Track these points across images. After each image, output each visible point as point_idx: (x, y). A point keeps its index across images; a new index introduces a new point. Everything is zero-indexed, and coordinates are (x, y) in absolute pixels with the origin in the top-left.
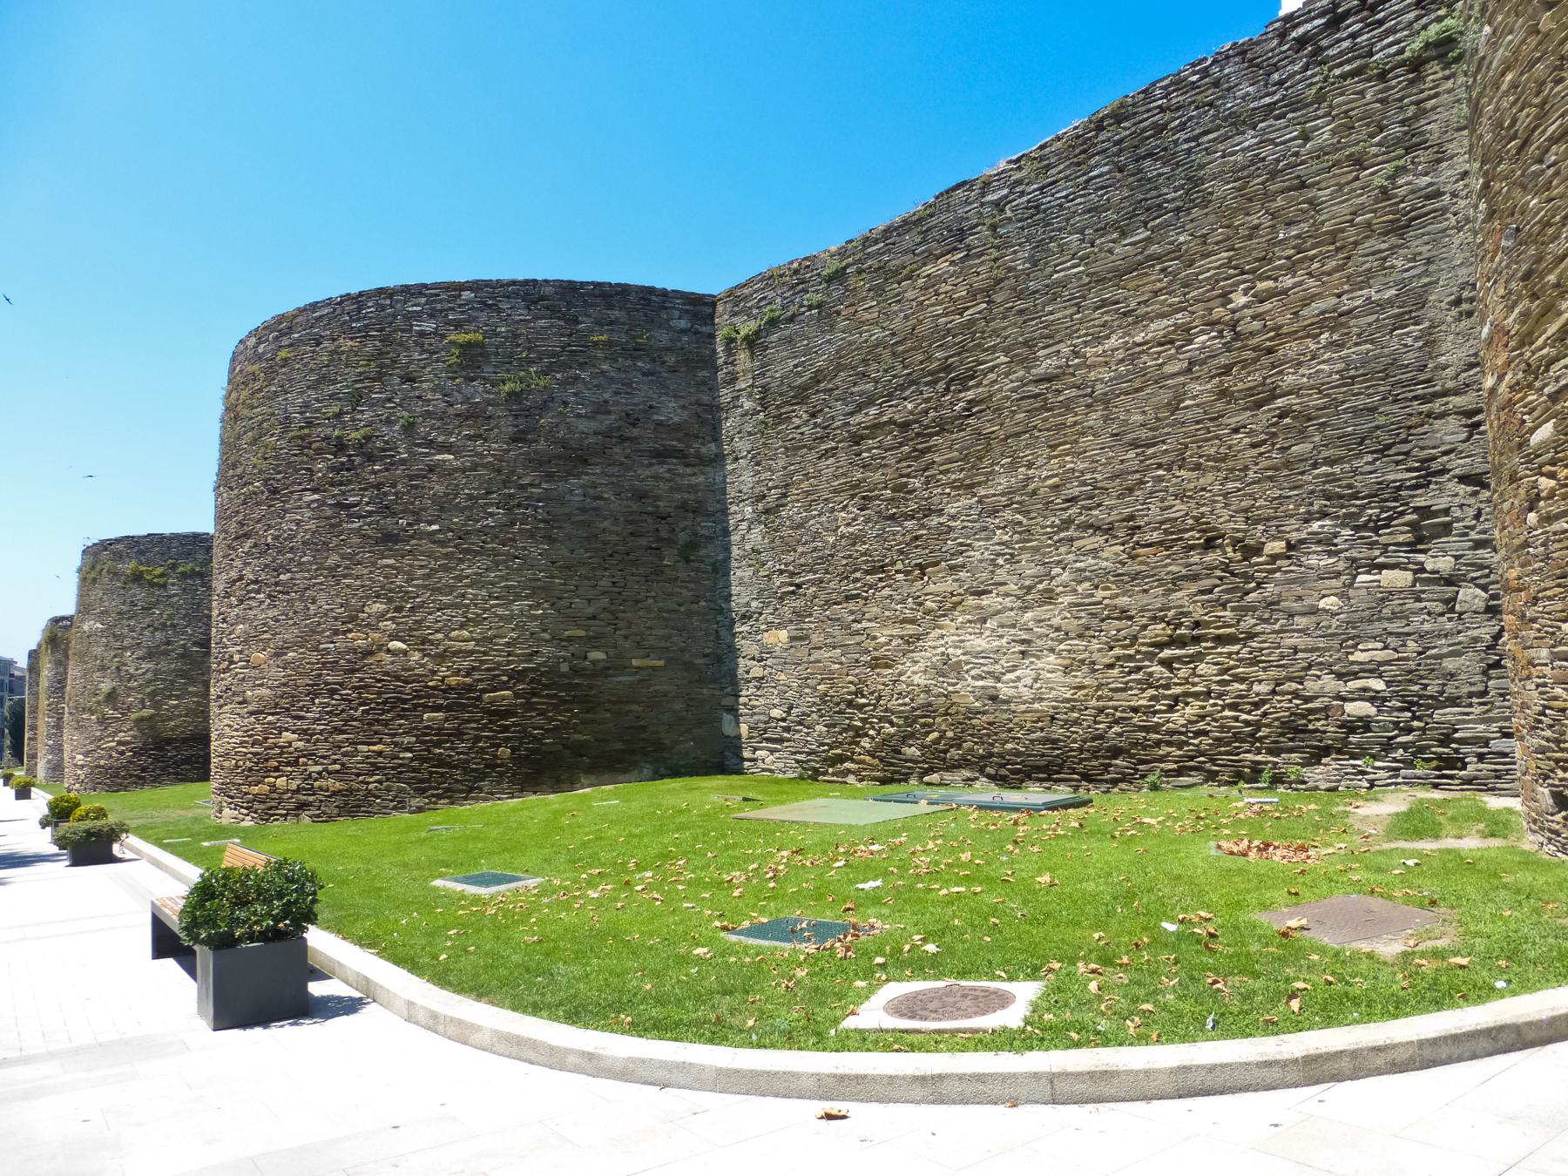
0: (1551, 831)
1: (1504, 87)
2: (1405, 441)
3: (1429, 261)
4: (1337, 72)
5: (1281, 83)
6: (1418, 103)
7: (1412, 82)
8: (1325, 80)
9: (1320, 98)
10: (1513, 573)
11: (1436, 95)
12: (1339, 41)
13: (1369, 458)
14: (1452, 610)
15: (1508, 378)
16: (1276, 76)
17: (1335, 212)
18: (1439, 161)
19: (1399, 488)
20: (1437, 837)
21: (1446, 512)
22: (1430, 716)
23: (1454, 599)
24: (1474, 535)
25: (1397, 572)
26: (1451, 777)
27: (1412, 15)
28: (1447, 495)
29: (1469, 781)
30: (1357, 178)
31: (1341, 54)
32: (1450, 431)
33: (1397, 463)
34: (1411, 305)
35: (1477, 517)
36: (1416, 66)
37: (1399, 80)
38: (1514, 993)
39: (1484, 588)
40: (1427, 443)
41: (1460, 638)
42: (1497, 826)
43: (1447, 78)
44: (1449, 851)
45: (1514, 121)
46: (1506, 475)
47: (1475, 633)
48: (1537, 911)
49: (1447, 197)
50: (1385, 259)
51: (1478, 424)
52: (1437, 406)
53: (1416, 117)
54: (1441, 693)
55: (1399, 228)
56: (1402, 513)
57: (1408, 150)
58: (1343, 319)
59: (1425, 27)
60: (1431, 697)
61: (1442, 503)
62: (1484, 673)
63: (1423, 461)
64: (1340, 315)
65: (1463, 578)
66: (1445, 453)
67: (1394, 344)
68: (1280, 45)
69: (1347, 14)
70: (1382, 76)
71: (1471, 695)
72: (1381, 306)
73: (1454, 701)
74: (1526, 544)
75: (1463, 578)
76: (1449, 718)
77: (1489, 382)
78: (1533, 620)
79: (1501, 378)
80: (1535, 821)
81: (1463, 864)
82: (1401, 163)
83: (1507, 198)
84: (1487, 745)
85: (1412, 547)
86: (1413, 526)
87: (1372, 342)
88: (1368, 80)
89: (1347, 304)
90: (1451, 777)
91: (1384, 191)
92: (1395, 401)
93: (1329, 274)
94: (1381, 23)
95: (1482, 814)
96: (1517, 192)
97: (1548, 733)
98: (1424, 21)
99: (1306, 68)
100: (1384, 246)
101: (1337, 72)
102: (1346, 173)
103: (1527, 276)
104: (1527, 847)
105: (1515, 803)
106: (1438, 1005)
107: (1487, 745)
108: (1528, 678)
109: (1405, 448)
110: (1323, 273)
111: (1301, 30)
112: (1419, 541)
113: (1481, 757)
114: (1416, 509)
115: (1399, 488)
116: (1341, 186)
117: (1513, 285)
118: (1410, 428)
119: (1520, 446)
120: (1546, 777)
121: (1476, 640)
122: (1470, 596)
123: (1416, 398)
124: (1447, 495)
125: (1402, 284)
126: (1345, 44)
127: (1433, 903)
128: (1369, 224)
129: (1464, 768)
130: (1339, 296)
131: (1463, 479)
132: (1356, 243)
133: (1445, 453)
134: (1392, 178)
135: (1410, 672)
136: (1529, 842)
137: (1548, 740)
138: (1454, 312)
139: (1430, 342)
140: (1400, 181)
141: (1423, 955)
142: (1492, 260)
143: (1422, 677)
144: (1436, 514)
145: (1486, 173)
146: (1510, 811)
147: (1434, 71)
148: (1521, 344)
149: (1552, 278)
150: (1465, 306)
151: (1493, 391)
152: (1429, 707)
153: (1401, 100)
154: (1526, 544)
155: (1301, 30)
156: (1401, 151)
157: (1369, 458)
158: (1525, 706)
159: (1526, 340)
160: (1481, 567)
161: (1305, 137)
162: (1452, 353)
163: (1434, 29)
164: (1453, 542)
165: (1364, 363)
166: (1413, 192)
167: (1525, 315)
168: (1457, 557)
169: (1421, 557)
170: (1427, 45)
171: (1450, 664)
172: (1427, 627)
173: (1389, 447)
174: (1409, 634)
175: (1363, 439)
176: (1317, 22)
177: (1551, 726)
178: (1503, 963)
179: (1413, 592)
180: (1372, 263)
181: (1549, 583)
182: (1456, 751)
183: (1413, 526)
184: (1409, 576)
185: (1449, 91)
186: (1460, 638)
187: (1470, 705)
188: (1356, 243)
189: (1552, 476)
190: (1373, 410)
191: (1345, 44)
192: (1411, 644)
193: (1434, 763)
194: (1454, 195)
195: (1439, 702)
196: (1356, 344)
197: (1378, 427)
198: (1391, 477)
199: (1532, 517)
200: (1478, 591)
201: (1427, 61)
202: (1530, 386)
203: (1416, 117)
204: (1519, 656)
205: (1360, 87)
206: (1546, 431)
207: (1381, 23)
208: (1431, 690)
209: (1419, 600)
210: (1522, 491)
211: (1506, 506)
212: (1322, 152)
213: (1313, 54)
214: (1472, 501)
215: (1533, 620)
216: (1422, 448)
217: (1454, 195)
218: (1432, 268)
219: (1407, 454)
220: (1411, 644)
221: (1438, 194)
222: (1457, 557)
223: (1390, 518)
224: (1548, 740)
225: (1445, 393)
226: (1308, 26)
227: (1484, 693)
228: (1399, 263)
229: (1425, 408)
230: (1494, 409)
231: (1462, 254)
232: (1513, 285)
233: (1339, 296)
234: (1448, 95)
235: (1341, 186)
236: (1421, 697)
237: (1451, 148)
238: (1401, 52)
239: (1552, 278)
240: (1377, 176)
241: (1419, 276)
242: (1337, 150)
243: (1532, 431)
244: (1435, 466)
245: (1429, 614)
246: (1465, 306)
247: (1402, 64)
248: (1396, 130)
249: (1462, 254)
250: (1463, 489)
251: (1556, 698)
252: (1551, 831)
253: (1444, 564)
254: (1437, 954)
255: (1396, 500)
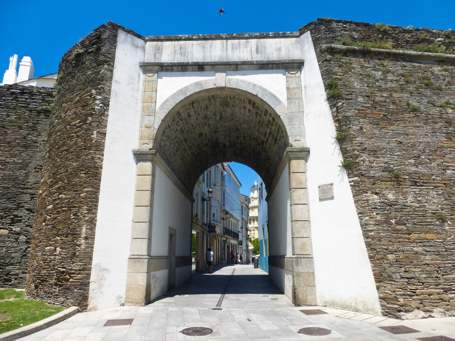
0: (33, 294)
1: (58, 134)
2: (15, 198)
3: (31, 157)
4: (20, 105)
5: (5, 100)
6: (37, 121)
7: (37, 116)
8: (17, 105)
9: (14, 108)
10: (37, 235)
11: (42, 121)
12: (22, 98)
13: (4, 200)
14: (17, 241)
15: (45, 193)
16: (4, 98)
17: (11, 137)
18: (39, 135)
19: (11, 209)
20: (3, 299)
21: (21, 217)
22: (5, 268)
23: (18, 239)
24: (27, 223)
25: (5, 230)
26: (7, 284)
27: (41, 101)
28: (22, 213)
29: (11, 285)
30: (19, 131)
31: (22, 101)
32: (27, 198)
33: (12, 203)
34: (24, 166)
35: (28, 219)
36: (39, 112)
37: (34, 113)
38: (24, 326)
39: (26, 236)
40: (20, 199)
41: (17, 248)
42: (19, 295)
43: (45, 118)
44: (7, 301)
45: (58, 142)
46: (40, 213)
47: (22, 247)
48: (29, 311)
49: (38, 144)
50: (21, 153)
51: (34, 197)
52: (25, 191)
53: (36, 124)
54: (9, 262)
55: (26, 147)
56: (10, 215)
57: (33, 130)
58: (6, 164)
59: (43, 105)
60: (6, 263)
61: (21, 214)
62: (22, 257)
63: (18, 203)
64: (6, 162)
65: (22, 233)
66: (24, 203)
67: (18, 174)
68: (7, 91)
69: (26, 93)
70: (31, 111)
71: (17, 263)
72: (17, 163)
73: (12, 264)
74: (41, 229)
75: (22, 233)
76: (10, 269)
77: (41, 192)
78: (39, 246)
79: (44, 192)
80: (29, 293)
81: (11, 304)
82: (30, 132)
83: (53, 156)
84: (18, 276)
85: (10, 224)
86: (12, 219)
87: (12, 171)
88: (27, 110)
89: (8, 160)
90: (7, 284)
91: (25, 137)
92: (15, 187)
93: (5, 151)
94: (33, 99)
95: (15, 292)
96: (56, 157)
97: (37, 272)
98: (43, 104)
99: (12, 100)
100: (21, 150)
101: (20, 105)
102: (17, 129)
103: (54, 174)
104: (26, 299)
105: (24, 290)
106: (8, 330)
107: (18, 276)
108: (35, 259)
109: (15, 199)
110: (4, 151)
111: (13, 90)
112: (13, 222)
113: (16, 279)
114: (14, 215)
115: (11, 209)
116: (14, 132)
117: (51, 174)
118: (17, 195)
119: (45, 208)
120: (34, 282)
121: (21, 249)
122: (22, 238)
123: (20, 188)
124: (22, 213)
125: (23, 160)
126: (24, 99)
127: (5, 312)
128: (19, 143)
129: (11, 282)
130: (7, 158)
131: (27, 210)
132: (14, 147)
133: (24, 203)
134: (27, 135)
135: (2, 256)
136: (26, 298)
137: (36, 273)
138: (34, 170)
139: (27, 175)
140: (29, 136)
141: (4, 322)
142: (47, 167)
143: (5, 258)
144: (18, 217)
145: (50, 148)
146: (22, 291)
147: (42, 116)
148: (49, 187)
149: (59, 176)
150: (37, 170)
151: (41, 194)
152: (5, 266)
153: (34, 118)
154: (41, 229)
155: (13, 90)
156: (31, 130)
157: (4, 200)
158: (33, 265)
159: (51, 186)
160: (27, 231)
161: (8, 116)
162: (32, 180)
163: (45, 107)
164: (21, 224)
165: (9, 176)
166: (31, 140)
167: (52, 181)
168: (21, 228)
169: (12, 227)
170: (42, 109)
171: (13, 255)
172: (9, 245)
173: (10, 198)
174: (4, 247)
175: (4, 195)
176: (18, 91)
177: (38, 270)
178: (22, 321)
179: (8, 236)
180: (17, 152)
181: (44, 239)
182: (10, 277)
183: (12, 219)
184: (8, 231)
185: (45, 121)
186: (17, 248)
187: (16, 265)
188: (14, 147)
189: (50, 216)
190: (8, 188)
191: (24, 99)
192: (4, 249)
193: (3, 281)
194: (40, 144)
195: (8, 265)
196: (8, 171)
197: (9, 193)
198: (9, 206)
199: (44, 224)
200: (25, 237)
201: (42, 113)
202: (50, 196)
203: (36, 124)
204: (34, 254)
205: (25, 111)
206: (51, 207)
207: (33, 99)
208: (7, 261)
209: (9, 238)
210: (43, 218)
211: (38, 220)
212: (11, 121)
213: (14, 97)
214: (28, 215)
215: (39, 246)
216: (19, 200)
217: (40, 144)
218: (32, 159)
219: (15, 201)
220: (4, 249)
221: (37, 143)
222: (21, 228)
223: (6, 216)
224: (36, 273)
225: (28, 188)
226: (16, 91)
227: (20, 262)
228: (24, 155)
229: (22, 191)
230: (40, 198)
231: (40, 155)
232: (51, 174)
233: (7, 158)
234: (44, 124)
235: (14, 132)
236: (3, 263)
237: (42, 134)
238: (36, 108)
239: (59, 176)
240: (24, 132)
241: (28, 160)
242: (15, 123)
243: (48, 206)
244: (21, 205)
245: (11, 242)
246: (37, 170)
247: (36, 111)
248: (31, 124)
249: (40, 155)
250: (27, 212)
251: (40, 264)
252: (33, 294)
253: (18, 229)
254: (7, 322)
255: (9, 212)
